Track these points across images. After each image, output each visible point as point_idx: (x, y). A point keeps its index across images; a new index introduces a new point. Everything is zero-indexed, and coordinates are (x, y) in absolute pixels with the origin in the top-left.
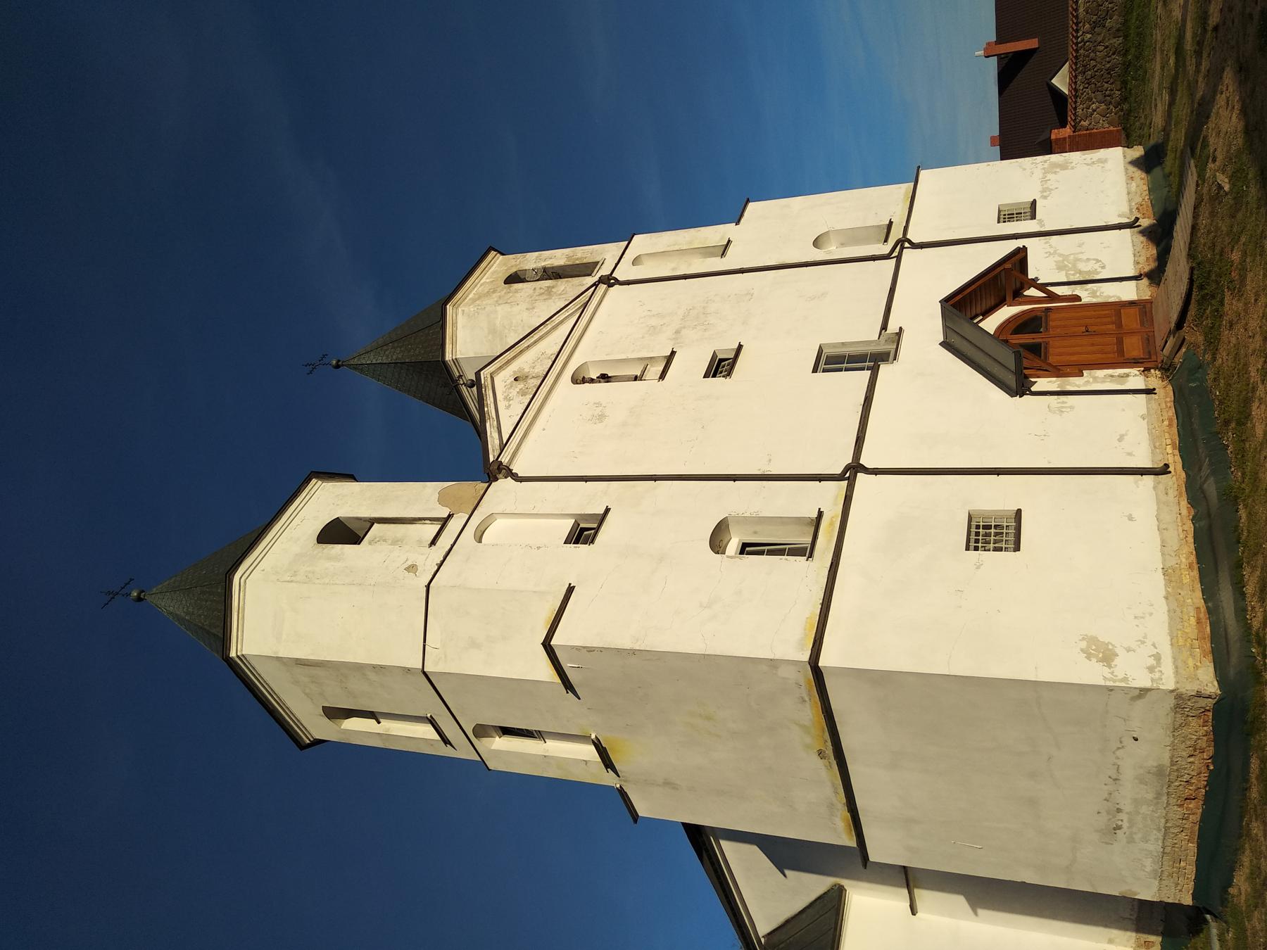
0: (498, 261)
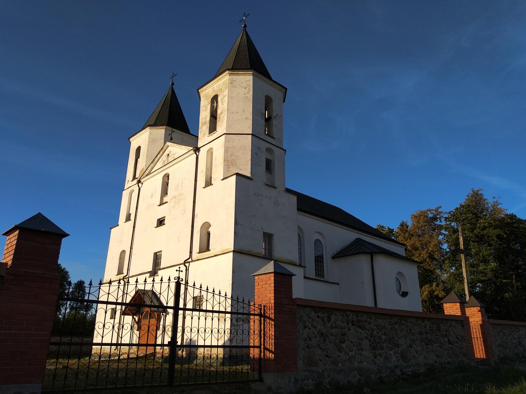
0: (224, 80)
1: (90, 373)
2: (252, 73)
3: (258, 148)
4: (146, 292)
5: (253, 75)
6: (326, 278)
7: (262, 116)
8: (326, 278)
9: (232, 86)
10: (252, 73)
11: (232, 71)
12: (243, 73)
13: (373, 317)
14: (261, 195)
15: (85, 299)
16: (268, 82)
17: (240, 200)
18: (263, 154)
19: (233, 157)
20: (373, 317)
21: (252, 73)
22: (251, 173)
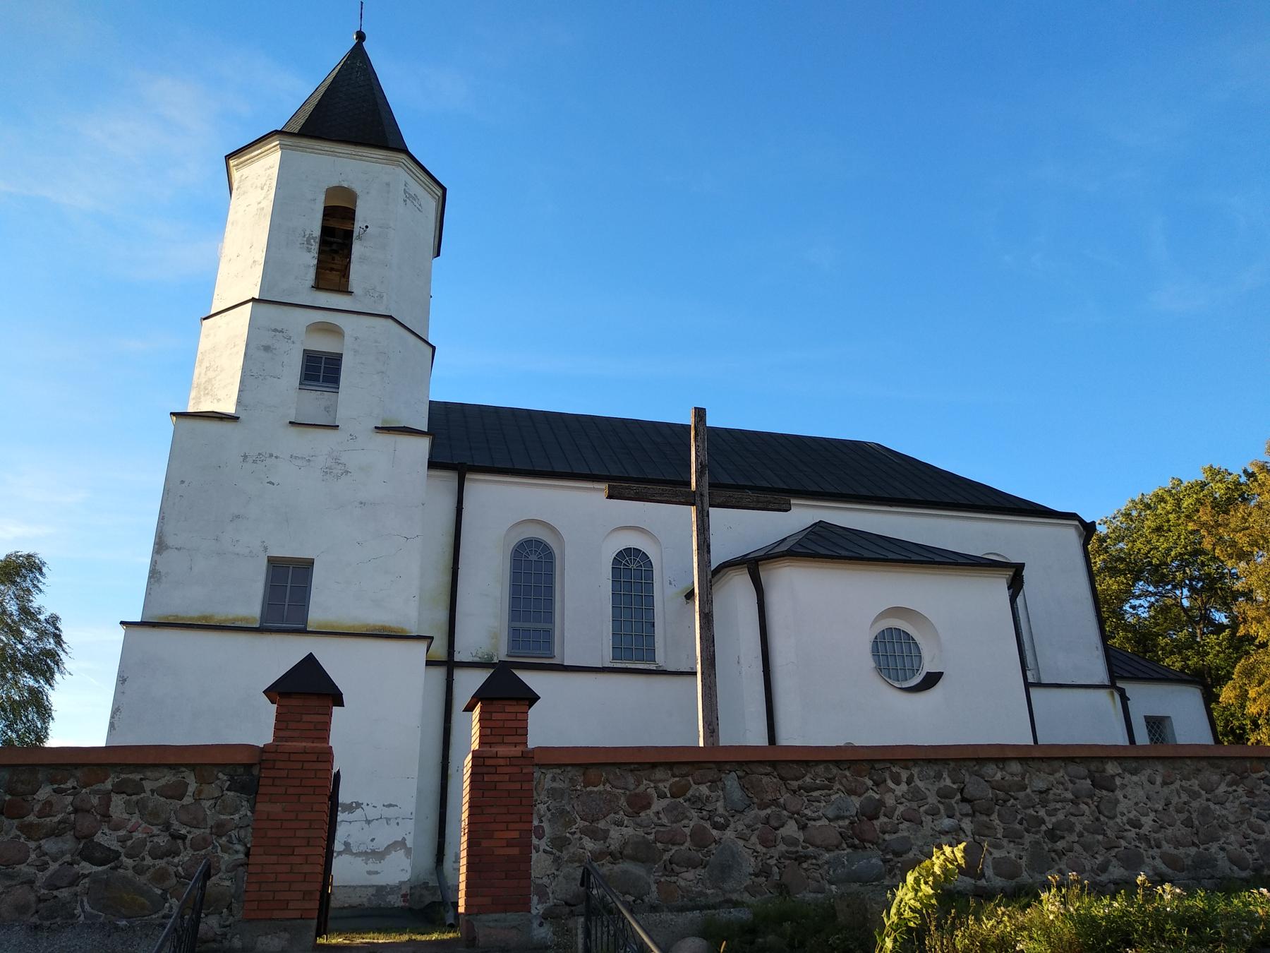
1: (343, 821)
2: (277, 145)
3: (275, 330)
4: (460, 676)
5: (281, 149)
6: (661, 660)
7: (308, 243)
8: (661, 660)
9: (239, 194)
10: (278, 142)
11: (239, 158)
12: (259, 151)
13: (455, 935)
14: (271, 455)
15: (53, 741)
16: (317, 147)
17: (183, 482)
18: (293, 343)
19: (211, 374)
20: (455, 935)
21: (278, 142)
22: (239, 402)
